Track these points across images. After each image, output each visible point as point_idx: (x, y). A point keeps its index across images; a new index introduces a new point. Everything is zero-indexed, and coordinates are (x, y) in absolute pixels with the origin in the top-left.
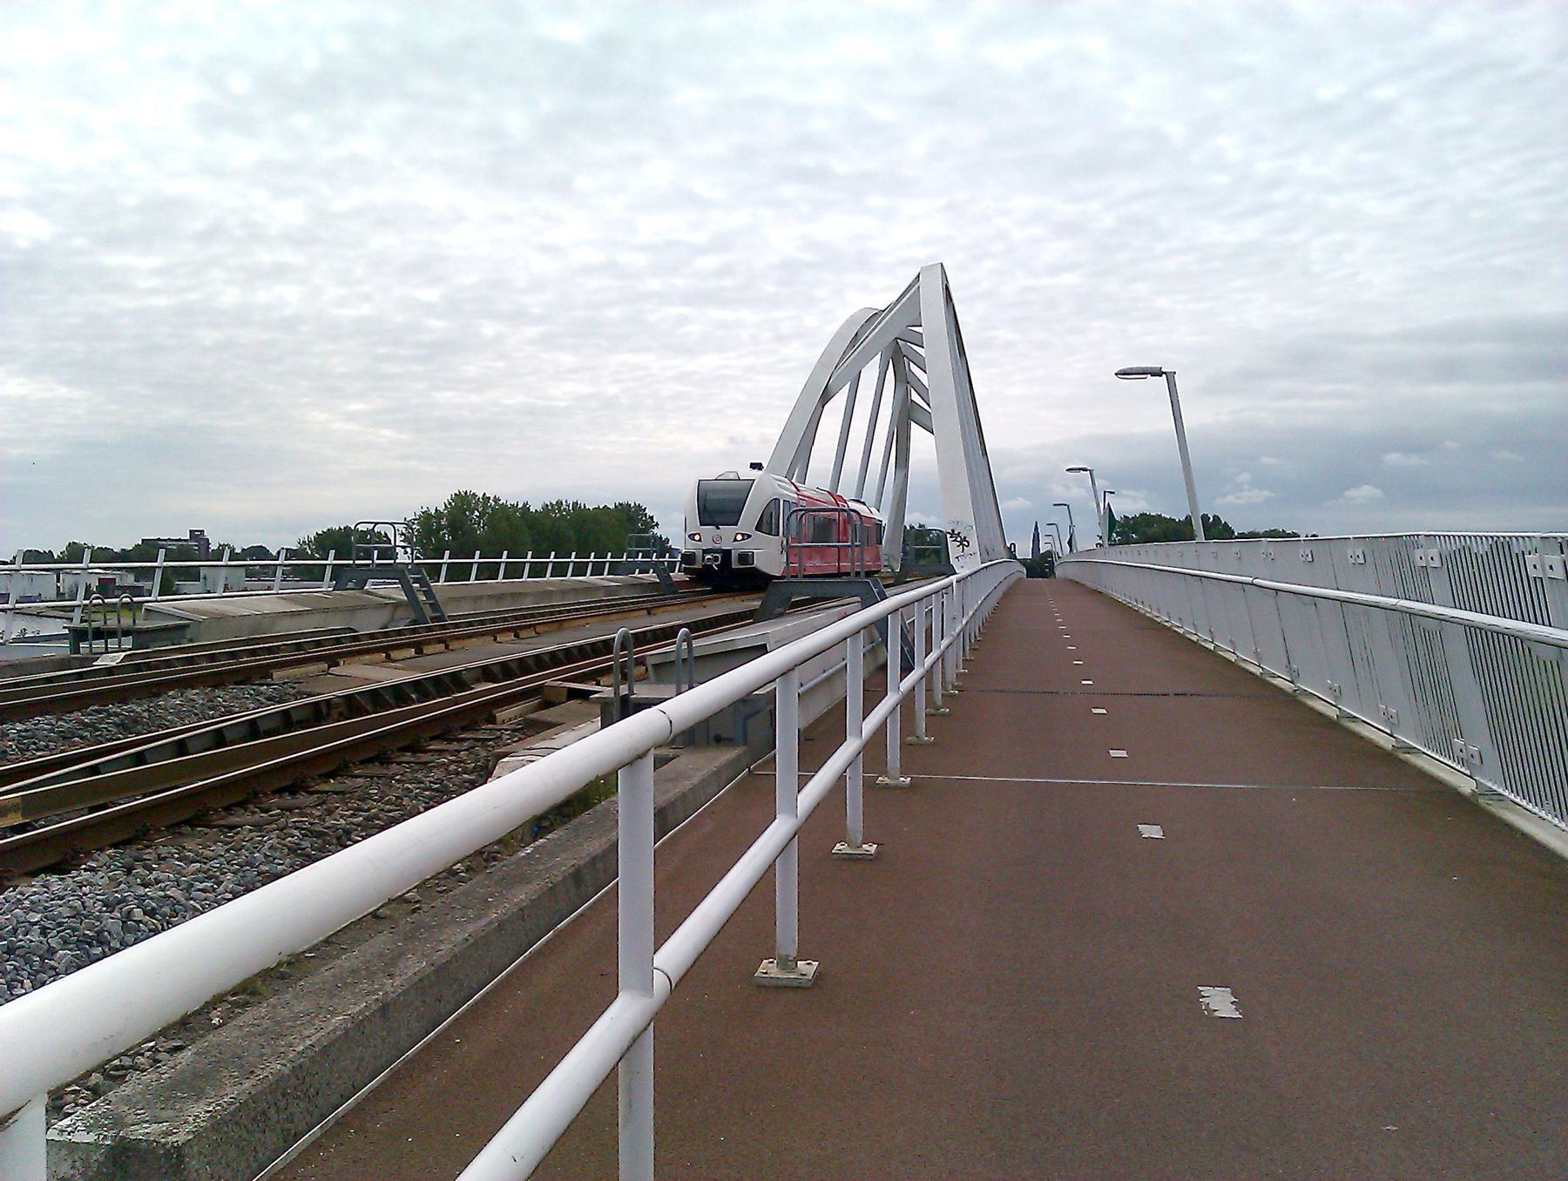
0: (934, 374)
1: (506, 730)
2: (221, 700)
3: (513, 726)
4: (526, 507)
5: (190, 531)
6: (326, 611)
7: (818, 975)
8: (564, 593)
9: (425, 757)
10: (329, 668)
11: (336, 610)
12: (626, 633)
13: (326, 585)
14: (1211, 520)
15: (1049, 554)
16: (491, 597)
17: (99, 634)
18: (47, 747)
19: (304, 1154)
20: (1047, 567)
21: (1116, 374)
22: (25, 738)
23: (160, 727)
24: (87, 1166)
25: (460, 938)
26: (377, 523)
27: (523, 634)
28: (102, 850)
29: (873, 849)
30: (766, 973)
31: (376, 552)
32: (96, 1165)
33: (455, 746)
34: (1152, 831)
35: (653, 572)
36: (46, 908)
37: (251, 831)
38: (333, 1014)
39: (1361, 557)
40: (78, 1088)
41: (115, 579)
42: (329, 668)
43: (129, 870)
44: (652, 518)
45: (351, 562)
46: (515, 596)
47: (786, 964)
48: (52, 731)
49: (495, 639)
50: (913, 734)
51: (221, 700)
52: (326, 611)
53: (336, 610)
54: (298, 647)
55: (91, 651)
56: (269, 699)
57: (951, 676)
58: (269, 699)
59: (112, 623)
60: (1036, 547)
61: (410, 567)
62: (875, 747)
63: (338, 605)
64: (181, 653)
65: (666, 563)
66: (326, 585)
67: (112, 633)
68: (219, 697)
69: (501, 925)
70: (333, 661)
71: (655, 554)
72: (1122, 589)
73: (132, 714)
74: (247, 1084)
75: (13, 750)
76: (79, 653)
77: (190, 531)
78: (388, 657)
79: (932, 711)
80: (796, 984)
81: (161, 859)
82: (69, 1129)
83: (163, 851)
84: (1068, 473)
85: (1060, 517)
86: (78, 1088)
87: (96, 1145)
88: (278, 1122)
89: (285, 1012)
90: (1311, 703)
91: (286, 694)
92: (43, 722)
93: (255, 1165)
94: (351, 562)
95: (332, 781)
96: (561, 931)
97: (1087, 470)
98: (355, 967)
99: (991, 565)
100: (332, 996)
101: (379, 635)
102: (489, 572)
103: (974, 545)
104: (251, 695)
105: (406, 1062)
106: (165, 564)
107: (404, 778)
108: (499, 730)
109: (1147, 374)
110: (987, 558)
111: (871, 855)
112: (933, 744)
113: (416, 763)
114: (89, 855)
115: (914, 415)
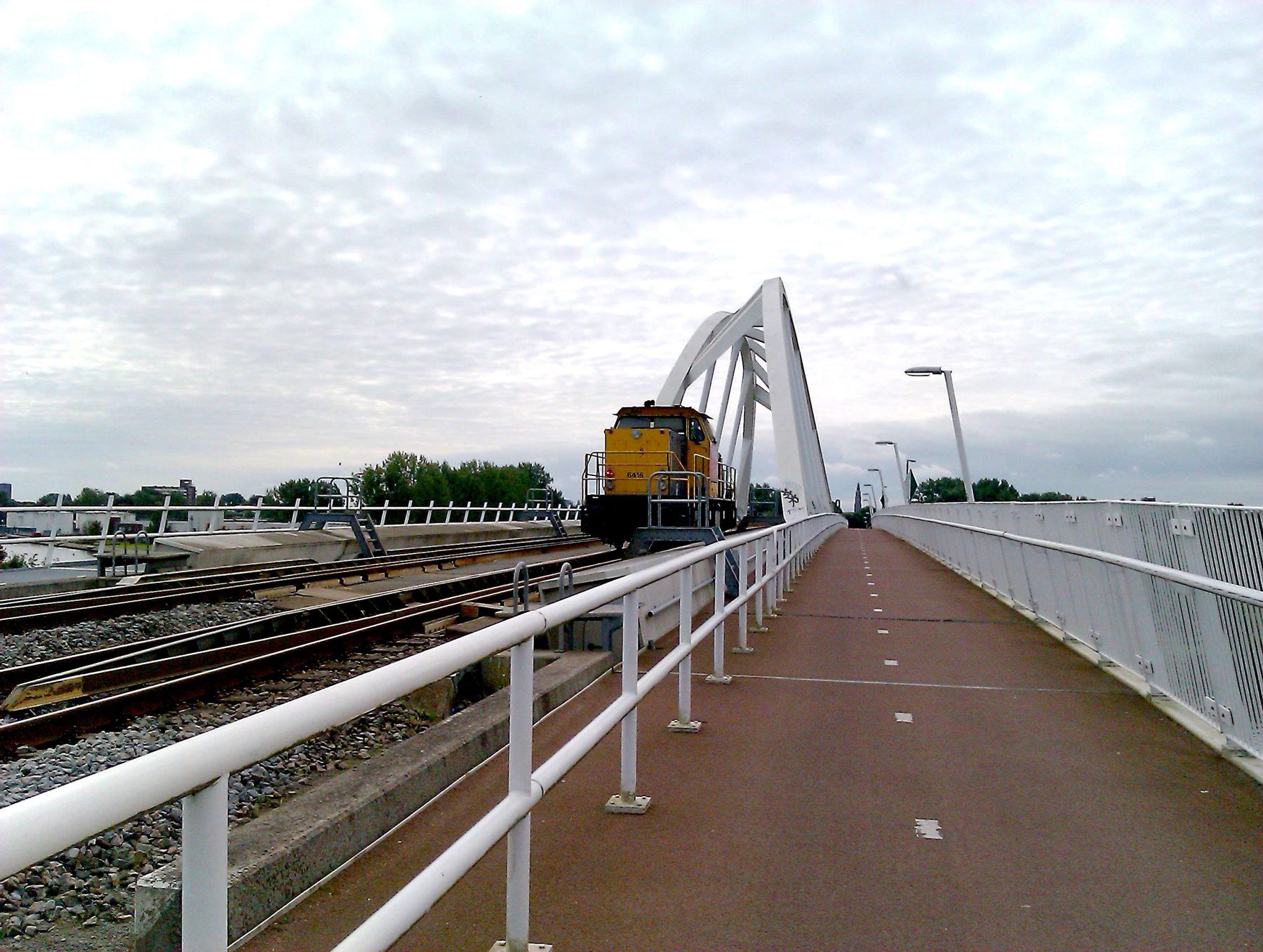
0: (773, 362)
1: (432, 638)
2: (217, 613)
3: (437, 635)
4: (445, 466)
5: (181, 481)
6: (293, 546)
7: (650, 808)
8: (477, 535)
9: (372, 656)
10: (297, 590)
11: (303, 545)
12: (524, 566)
13: (293, 525)
14: (1000, 484)
15: (867, 509)
16: (420, 537)
17: (122, 561)
18: (90, 644)
19: (299, 907)
20: (866, 520)
21: (906, 372)
22: (75, 638)
23: (172, 632)
24: (163, 904)
25: (402, 774)
26: (334, 479)
27: (445, 566)
28: (142, 717)
29: (698, 725)
30: (613, 804)
31: (332, 500)
32: (169, 902)
33: (394, 648)
34: (904, 717)
35: (548, 519)
36: (109, 753)
37: (248, 705)
38: (318, 818)
39: (1119, 520)
40: (135, 873)
41: (119, 518)
42: (297, 590)
43: (163, 730)
44: (548, 475)
45: (313, 508)
46: (440, 537)
47: (627, 797)
48: (93, 633)
49: (424, 570)
50: (737, 645)
51: (217, 613)
52: (293, 546)
53: (303, 545)
54: (273, 574)
55: (114, 574)
56: (252, 612)
57: (772, 602)
58: (252, 612)
59: (131, 552)
60: (858, 503)
61: (358, 512)
62: (702, 652)
63: (305, 541)
64: (186, 577)
65: (558, 513)
66: (293, 525)
67: (130, 561)
68: (216, 610)
69: (430, 769)
70: (299, 584)
71: (550, 505)
72: (914, 537)
73: (152, 622)
74: (263, 858)
75: (66, 646)
76: (104, 576)
77: (181, 481)
78: (342, 582)
79: (755, 629)
80: (633, 812)
81: (184, 723)
82: (152, 880)
83: (187, 718)
84: (879, 446)
85: (874, 479)
86: (135, 873)
87: (169, 890)
88: (282, 884)
89: (286, 817)
90: (1047, 629)
91: (265, 609)
92: (87, 626)
93: (268, 910)
94: (313, 508)
95: (304, 672)
96: (472, 775)
97: (891, 444)
98: (330, 791)
99: (815, 517)
100: (316, 808)
101: (335, 566)
102: (419, 517)
103: (803, 502)
104: (239, 609)
105: (364, 854)
106: (488, 509)
107: (357, 671)
108: (427, 638)
109: (930, 372)
110: (813, 511)
111: (696, 729)
112: (752, 653)
113: (365, 661)
114: (134, 720)
115: (758, 396)
